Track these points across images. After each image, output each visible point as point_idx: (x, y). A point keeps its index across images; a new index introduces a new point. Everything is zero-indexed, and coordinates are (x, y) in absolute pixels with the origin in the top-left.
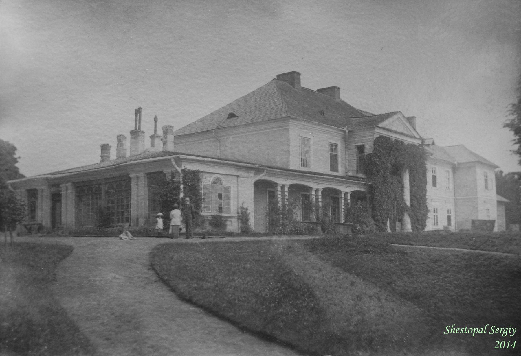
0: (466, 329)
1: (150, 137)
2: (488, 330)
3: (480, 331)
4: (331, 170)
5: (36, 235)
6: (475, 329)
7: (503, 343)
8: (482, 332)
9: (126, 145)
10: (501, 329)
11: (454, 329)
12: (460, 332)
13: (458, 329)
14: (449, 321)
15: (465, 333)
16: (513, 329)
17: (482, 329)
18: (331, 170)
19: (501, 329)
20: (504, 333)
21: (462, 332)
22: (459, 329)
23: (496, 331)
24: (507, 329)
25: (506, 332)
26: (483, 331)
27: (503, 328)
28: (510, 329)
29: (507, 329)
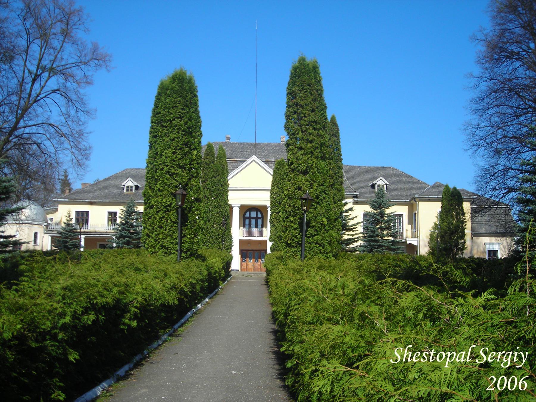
0: (432, 353)
1: (108, 212)
2: (474, 356)
3: (451, 357)
4: (87, 213)
5: (74, 37)
6: (449, 353)
7: (501, 386)
8: (462, 360)
9: (87, 30)
10: (500, 354)
11: (410, 353)
12: (422, 359)
13: (418, 354)
14: (9, 138)
15: (431, 360)
16: (521, 353)
17: (464, 353)
18: (87, 213)
19: (500, 353)
20: (505, 360)
21: (424, 358)
22: (419, 353)
23: (490, 357)
24: (511, 353)
25: (509, 359)
26: (465, 357)
27: (504, 352)
28: (516, 353)
29: (511, 353)
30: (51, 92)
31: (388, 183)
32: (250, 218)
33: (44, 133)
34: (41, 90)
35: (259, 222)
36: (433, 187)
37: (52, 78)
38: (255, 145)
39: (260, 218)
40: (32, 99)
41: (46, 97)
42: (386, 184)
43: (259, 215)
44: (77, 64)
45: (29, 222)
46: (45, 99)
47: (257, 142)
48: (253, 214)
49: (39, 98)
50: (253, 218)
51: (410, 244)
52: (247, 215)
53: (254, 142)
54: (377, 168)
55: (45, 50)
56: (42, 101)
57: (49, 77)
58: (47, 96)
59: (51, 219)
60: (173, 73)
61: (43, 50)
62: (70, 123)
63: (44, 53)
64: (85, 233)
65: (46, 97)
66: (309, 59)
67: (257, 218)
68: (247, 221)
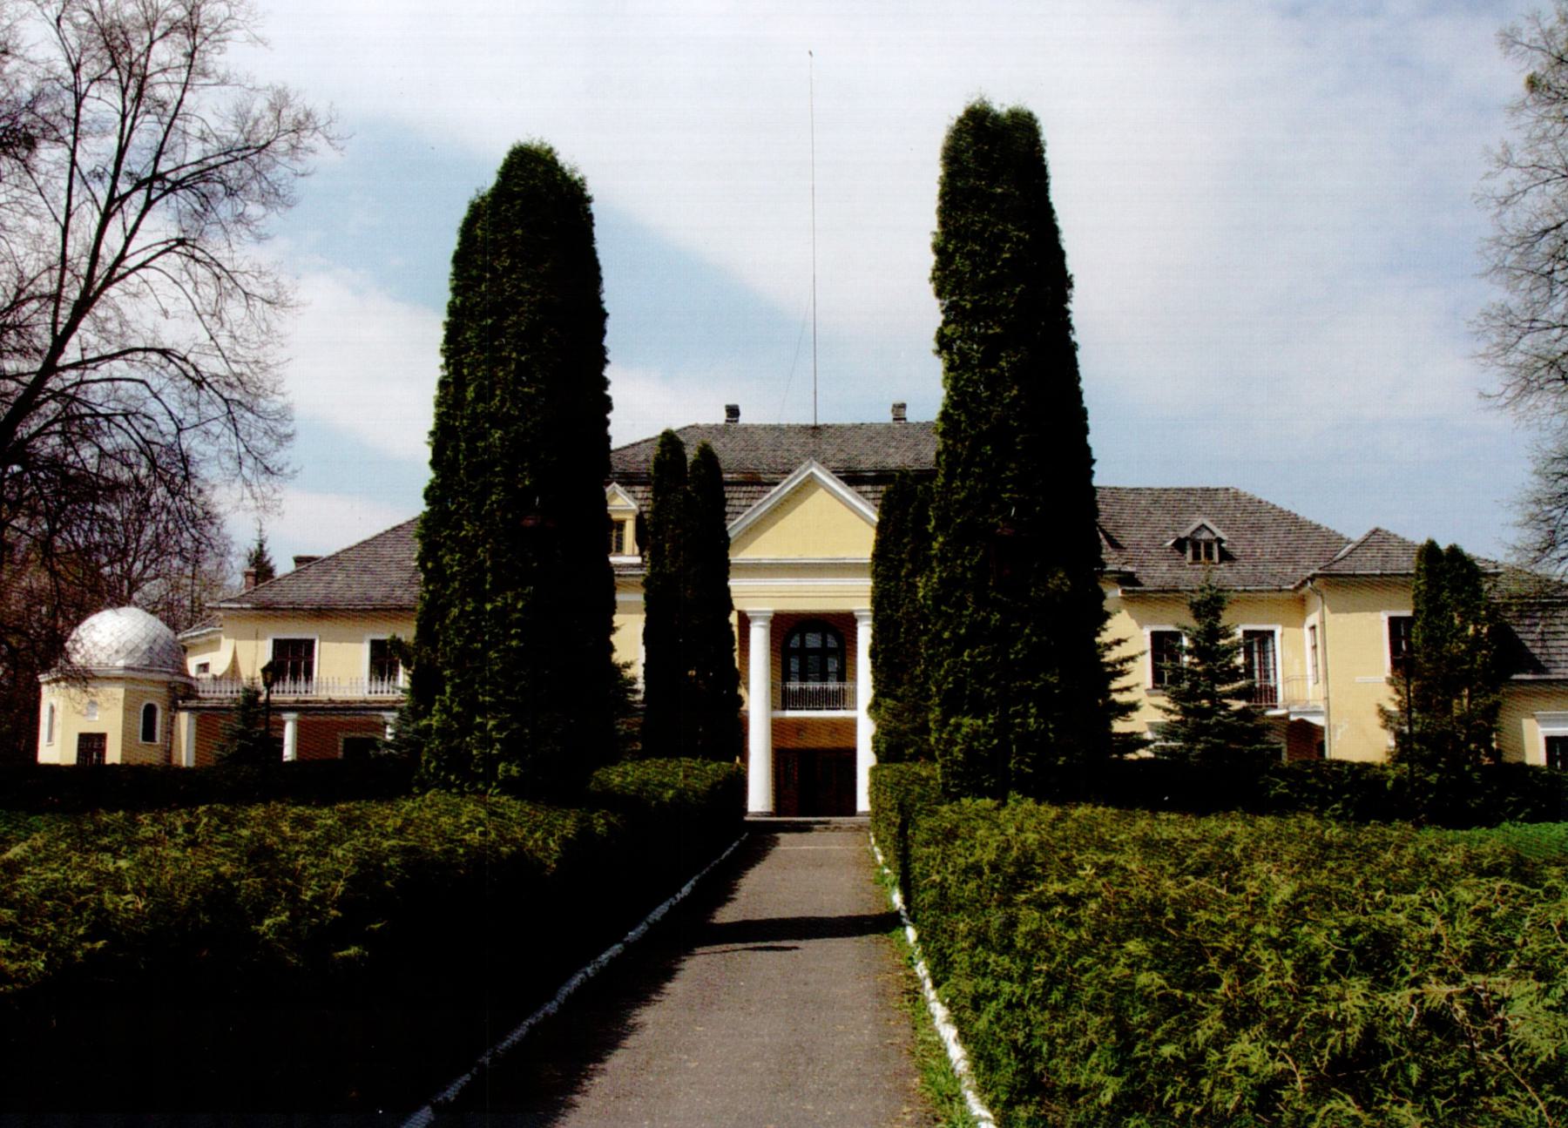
30: (161, 248)
31: (1225, 537)
32: (803, 652)
33: (138, 376)
34: (128, 240)
35: (833, 665)
36: (1364, 544)
37: (159, 203)
38: (816, 428)
39: (833, 652)
40: (101, 272)
41: (143, 265)
42: (1220, 541)
43: (832, 643)
44: (235, 154)
45: (342, 718)
46: (141, 272)
47: (820, 422)
48: (813, 641)
49: (120, 271)
50: (814, 651)
51: (1302, 722)
52: (795, 642)
53: (811, 422)
54: (1189, 492)
55: (134, 118)
56: (132, 278)
57: (149, 204)
58: (151, 264)
59: (204, 667)
60: (577, 1098)
61: (129, 122)
62: (224, 341)
63: (132, 128)
64: (301, 708)
65: (143, 265)
66: (1001, 104)
67: (824, 652)
68: (795, 666)
